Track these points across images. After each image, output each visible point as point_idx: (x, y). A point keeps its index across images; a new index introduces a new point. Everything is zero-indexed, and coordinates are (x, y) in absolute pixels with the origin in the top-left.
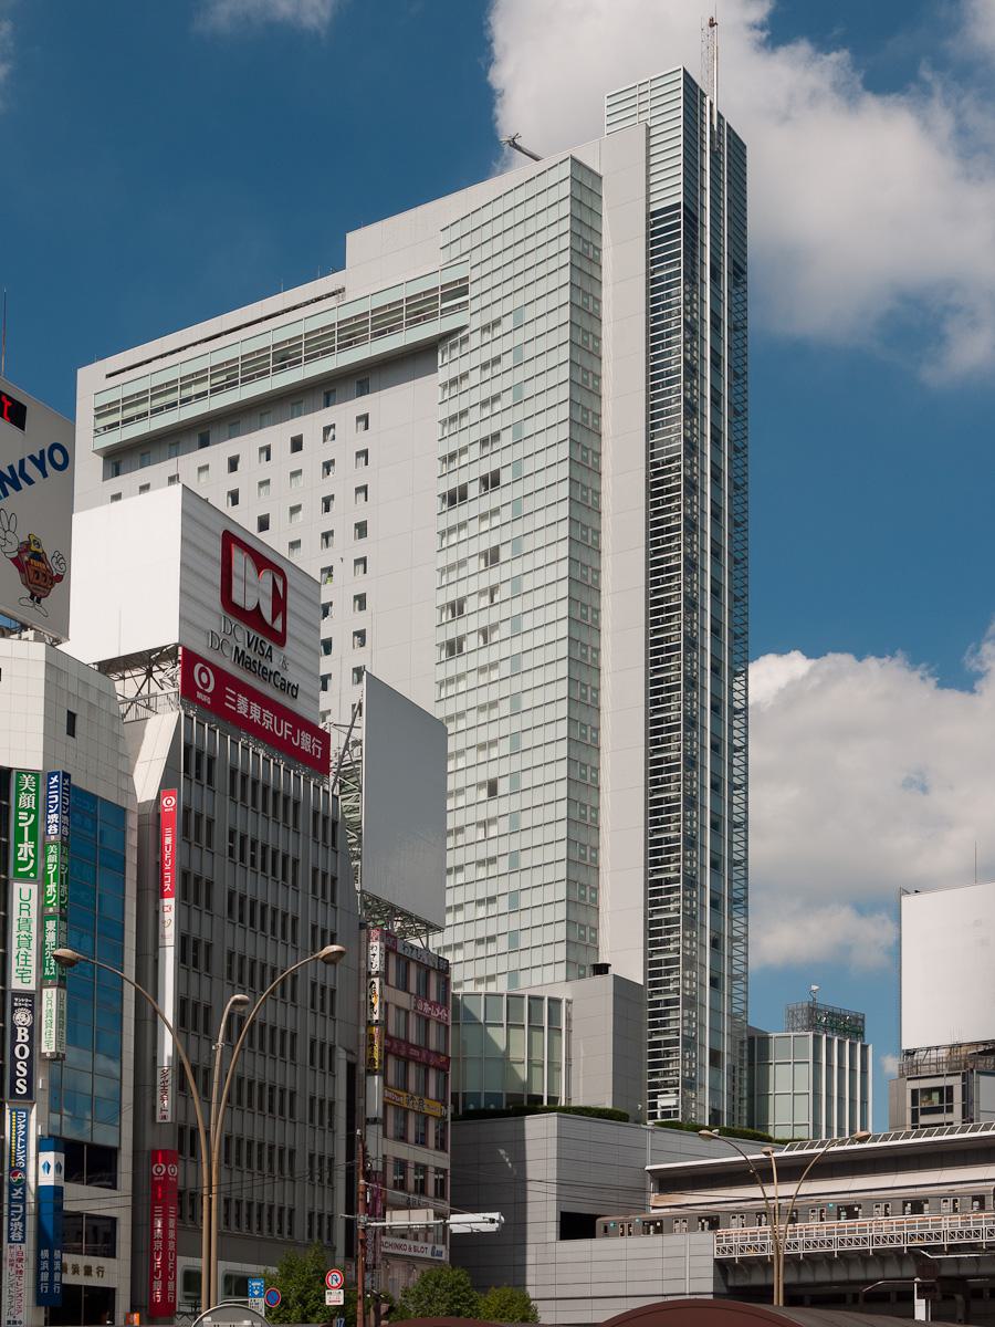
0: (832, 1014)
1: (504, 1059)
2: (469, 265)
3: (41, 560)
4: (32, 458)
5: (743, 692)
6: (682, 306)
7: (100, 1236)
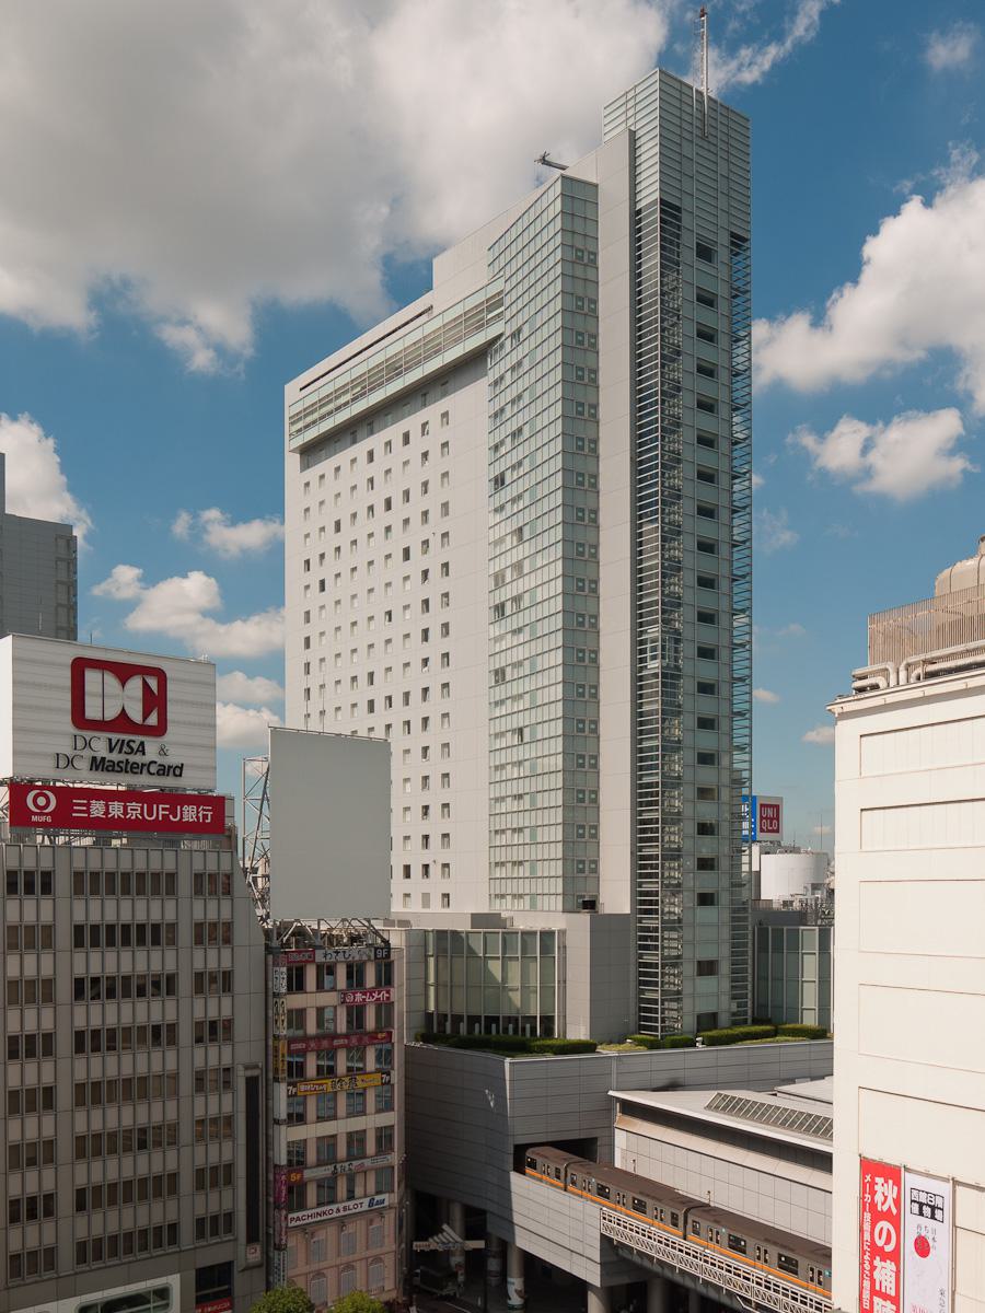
1: (503, 987)
2: (503, 280)
6: (659, 297)
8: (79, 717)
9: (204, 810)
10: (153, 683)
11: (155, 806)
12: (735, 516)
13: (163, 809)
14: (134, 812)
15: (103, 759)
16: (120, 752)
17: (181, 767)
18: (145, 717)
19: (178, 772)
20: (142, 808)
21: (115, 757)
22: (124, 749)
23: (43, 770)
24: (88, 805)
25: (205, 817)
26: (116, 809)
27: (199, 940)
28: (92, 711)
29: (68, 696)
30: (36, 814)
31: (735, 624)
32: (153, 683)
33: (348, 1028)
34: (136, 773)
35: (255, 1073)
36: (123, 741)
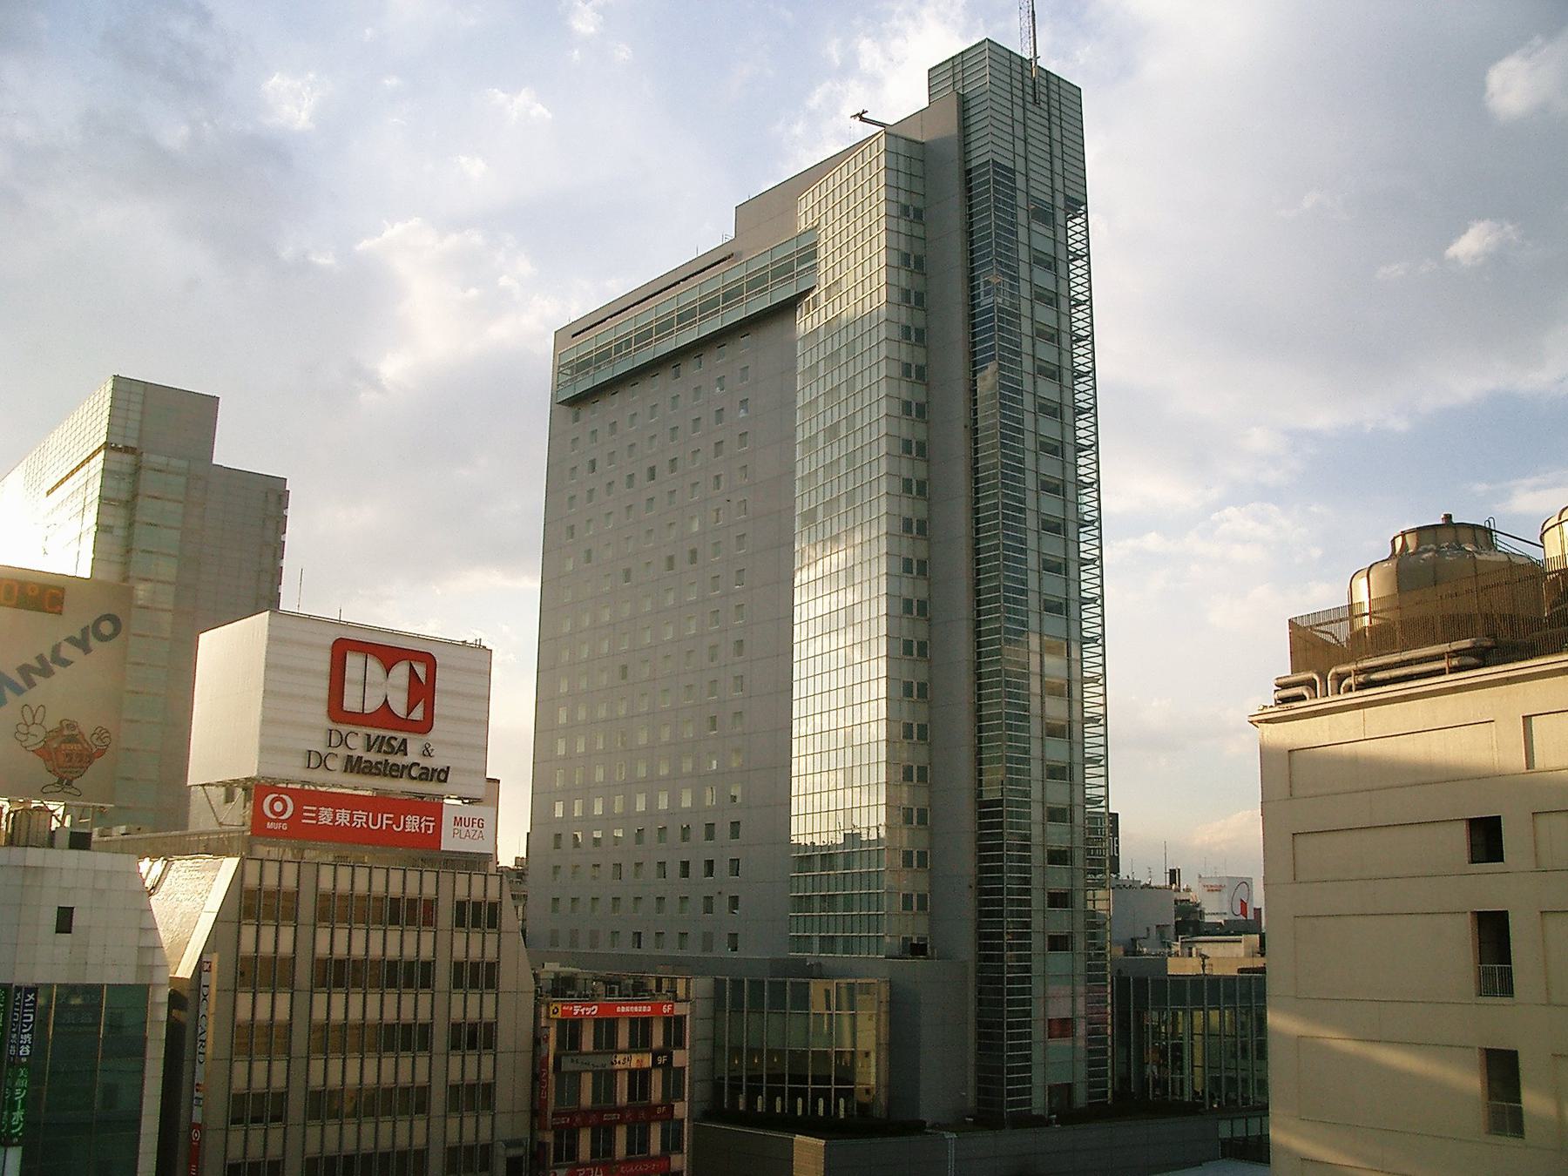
0: (1412, 665)
3: (77, 742)
4: (71, 640)
5: (1084, 233)
7: (848, 907)
8: (336, 710)
9: (426, 821)
10: (421, 670)
11: (380, 815)
12: (1082, 530)
13: (387, 818)
14: (360, 821)
15: (360, 758)
16: (379, 751)
17: (446, 771)
18: (410, 710)
19: (442, 777)
20: (368, 816)
21: (373, 757)
22: (383, 748)
23: (292, 770)
24: (317, 812)
25: (427, 827)
26: (361, 819)
27: (457, 983)
28: (351, 702)
29: (326, 684)
30: (272, 820)
31: (1084, 615)
32: (421, 670)
33: (629, 1099)
34: (396, 777)
35: (518, 1152)
36: (384, 737)
